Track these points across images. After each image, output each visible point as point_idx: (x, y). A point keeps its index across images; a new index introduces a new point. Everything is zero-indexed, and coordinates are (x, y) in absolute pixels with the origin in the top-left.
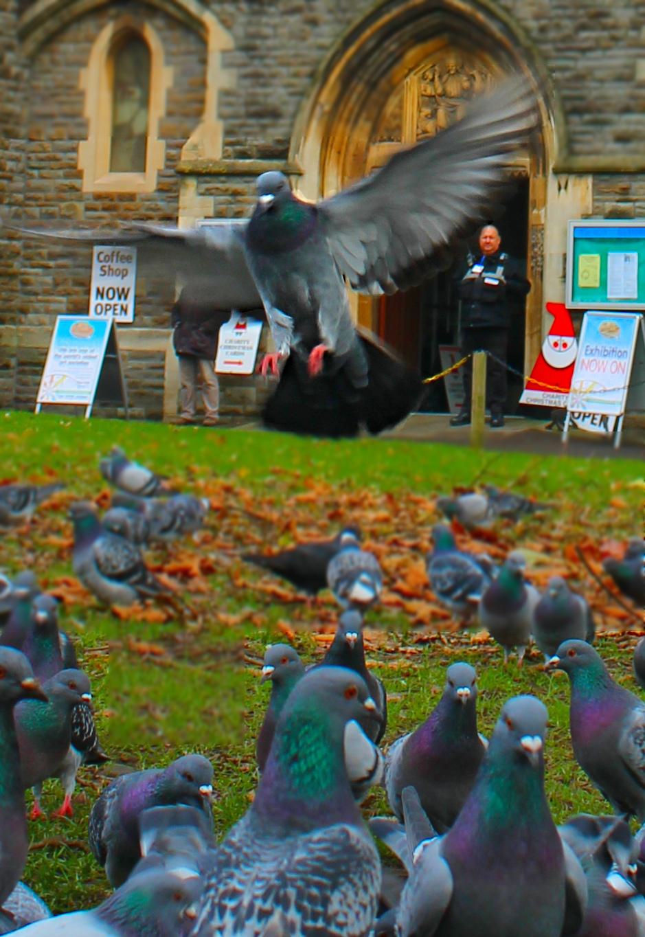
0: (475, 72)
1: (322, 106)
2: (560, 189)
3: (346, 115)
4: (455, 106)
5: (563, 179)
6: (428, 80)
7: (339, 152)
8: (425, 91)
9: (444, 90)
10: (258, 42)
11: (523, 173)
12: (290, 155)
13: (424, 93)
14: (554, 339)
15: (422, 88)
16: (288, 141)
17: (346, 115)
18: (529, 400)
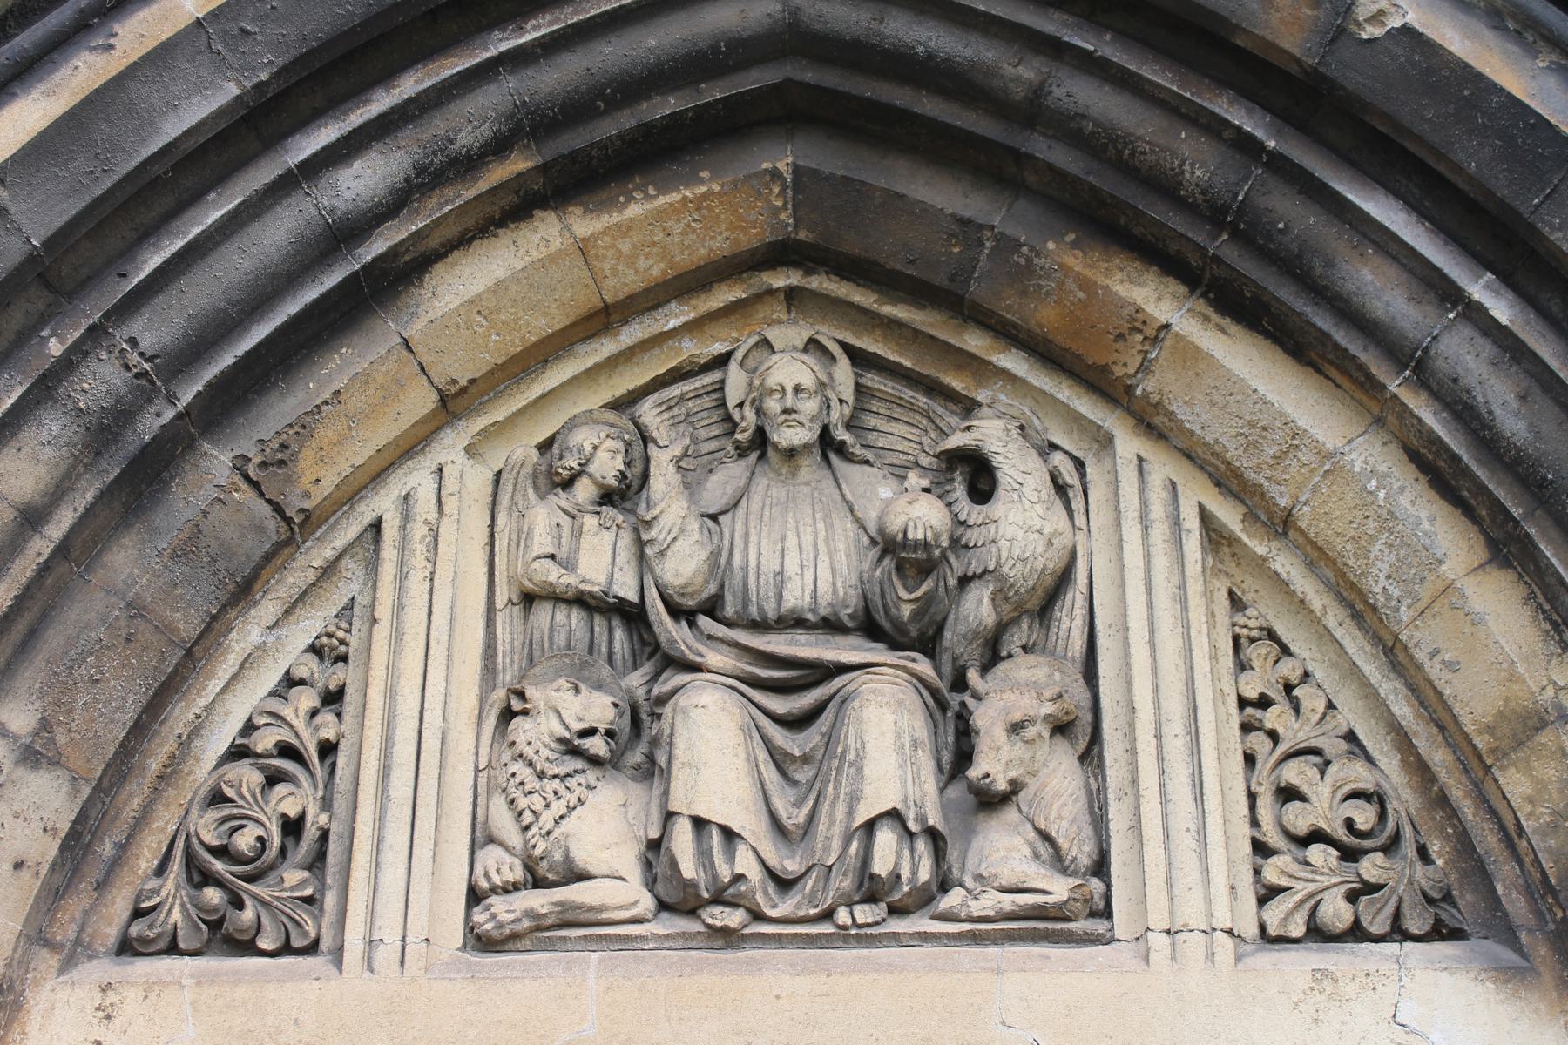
6: (584, 491)
8: (569, 565)
9: (718, 563)
13: (553, 575)
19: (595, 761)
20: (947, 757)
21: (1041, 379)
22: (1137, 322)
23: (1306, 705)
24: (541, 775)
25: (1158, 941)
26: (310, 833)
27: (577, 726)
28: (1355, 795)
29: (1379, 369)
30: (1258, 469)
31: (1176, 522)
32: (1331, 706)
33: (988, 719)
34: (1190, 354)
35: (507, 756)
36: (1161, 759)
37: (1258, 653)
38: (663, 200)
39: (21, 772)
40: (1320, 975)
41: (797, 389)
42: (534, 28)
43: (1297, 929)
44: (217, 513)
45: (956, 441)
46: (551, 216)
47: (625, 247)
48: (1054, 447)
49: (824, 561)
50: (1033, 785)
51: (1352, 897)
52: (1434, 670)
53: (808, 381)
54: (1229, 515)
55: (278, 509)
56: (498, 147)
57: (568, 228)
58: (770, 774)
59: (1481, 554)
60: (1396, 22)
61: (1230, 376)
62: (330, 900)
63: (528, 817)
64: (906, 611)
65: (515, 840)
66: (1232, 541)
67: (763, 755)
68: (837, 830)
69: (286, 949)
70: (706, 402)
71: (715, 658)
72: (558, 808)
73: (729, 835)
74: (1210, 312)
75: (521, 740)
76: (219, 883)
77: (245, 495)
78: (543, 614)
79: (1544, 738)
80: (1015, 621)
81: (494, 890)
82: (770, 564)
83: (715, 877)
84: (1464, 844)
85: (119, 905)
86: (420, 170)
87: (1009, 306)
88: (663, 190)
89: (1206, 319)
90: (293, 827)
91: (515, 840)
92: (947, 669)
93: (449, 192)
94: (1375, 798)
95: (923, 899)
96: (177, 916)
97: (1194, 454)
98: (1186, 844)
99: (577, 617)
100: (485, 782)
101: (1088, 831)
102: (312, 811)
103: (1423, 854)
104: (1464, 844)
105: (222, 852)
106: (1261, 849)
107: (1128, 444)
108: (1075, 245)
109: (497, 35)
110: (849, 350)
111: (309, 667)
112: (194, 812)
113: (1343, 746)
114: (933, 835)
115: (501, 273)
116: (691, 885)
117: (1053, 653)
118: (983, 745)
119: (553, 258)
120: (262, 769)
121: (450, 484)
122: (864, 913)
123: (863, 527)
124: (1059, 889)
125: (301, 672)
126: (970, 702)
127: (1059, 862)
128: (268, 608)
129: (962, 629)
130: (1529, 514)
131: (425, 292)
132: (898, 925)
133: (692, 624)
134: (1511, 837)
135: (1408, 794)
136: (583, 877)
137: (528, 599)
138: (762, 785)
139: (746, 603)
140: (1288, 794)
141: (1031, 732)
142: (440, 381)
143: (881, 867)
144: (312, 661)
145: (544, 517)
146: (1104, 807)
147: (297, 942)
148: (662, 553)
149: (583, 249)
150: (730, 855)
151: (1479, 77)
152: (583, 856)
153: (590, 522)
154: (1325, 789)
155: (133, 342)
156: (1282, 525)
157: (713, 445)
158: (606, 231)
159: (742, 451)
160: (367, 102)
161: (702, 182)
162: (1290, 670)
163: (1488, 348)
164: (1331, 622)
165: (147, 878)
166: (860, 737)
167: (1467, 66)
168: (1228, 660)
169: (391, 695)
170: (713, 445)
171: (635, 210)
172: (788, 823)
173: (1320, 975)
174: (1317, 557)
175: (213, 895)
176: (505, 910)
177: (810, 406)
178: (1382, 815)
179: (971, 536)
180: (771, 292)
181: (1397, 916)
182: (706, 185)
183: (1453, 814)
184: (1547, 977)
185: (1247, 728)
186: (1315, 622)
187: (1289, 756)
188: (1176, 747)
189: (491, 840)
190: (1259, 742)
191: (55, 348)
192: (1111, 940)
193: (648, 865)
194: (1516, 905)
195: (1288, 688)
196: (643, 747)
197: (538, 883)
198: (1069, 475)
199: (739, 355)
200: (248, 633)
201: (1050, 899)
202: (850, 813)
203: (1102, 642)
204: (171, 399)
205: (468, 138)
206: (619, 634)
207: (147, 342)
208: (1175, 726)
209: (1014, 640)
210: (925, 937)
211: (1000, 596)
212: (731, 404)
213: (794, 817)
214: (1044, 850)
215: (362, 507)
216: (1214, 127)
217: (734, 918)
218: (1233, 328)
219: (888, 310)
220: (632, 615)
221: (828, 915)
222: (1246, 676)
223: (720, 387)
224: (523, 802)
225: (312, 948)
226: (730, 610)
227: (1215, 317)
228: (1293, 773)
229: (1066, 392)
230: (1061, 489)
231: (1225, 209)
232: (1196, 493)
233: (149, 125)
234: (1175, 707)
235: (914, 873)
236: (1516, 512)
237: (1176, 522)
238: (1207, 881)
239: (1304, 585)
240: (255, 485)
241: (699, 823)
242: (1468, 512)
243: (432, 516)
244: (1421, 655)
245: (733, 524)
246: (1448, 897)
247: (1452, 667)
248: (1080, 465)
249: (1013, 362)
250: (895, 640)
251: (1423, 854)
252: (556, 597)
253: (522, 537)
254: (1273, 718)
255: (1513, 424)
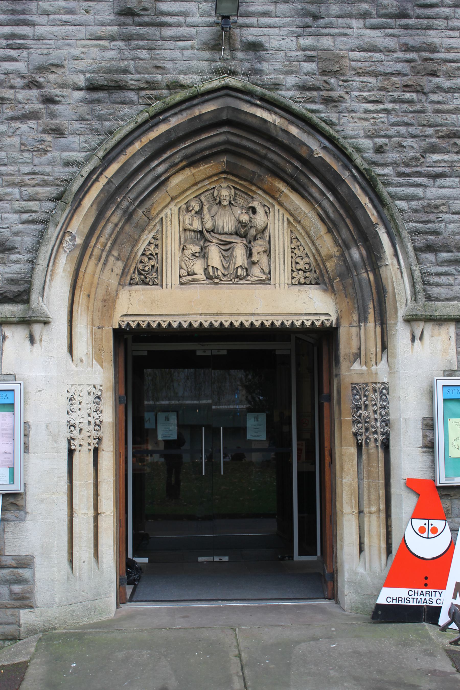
0: (256, 204)
1: (74, 238)
2: (413, 339)
3: (97, 252)
4: (230, 243)
5: (418, 327)
6: (193, 212)
7: (89, 296)
8: (191, 225)
9: (214, 224)
10: (300, 30)
11: (326, 322)
12: (35, 297)
13: (190, 227)
14: (418, 523)
15: (187, 222)
16: (29, 281)
17: (97, 252)
18: (389, 600)
19: (197, 257)
20: (248, 255)
21: (264, 195)
22: (279, 190)
23: (300, 249)
24: (189, 259)
25: (277, 285)
26: (156, 267)
27: (194, 252)
28: (306, 263)
29: (314, 203)
30: (296, 214)
31: (283, 220)
32: (304, 249)
33: (254, 251)
34: (286, 196)
35: (184, 256)
36: (279, 258)
37: (294, 241)
38: (206, 166)
39: (117, 262)
40: (299, 290)
41: (226, 196)
42: (188, 143)
43: (297, 283)
44: (140, 220)
45: (250, 205)
46: (188, 169)
47: (200, 174)
48: (265, 206)
49: (230, 224)
50: (260, 261)
51: (305, 278)
52: (318, 247)
53: (228, 194)
54: (291, 219)
55: (148, 218)
56: (181, 161)
57: (191, 171)
58: (223, 259)
59: (327, 231)
60: (319, 155)
61: (292, 200)
62: (159, 277)
63: (188, 266)
64: (242, 232)
65: (186, 269)
66: (291, 223)
67: (221, 256)
68: (232, 268)
69: (154, 284)
70: (211, 195)
71: (214, 241)
72: (192, 264)
73: (217, 269)
74: (290, 189)
75: (186, 254)
76: (143, 275)
77: (144, 217)
78: (188, 233)
79: (332, 259)
80: (259, 234)
81: (183, 276)
82: (222, 225)
83: (215, 275)
84: (321, 271)
85: (129, 278)
86: (170, 166)
87: (259, 184)
88: (206, 165)
89: (290, 190)
90: (153, 266)
91: (186, 269)
92: (248, 241)
93: (174, 168)
94: (309, 264)
95: (244, 278)
96: (137, 280)
97: (286, 209)
98: (282, 271)
99: (193, 233)
100: (181, 260)
101: (268, 267)
102: (155, 264)
103: (315, 272)
104: (321, 271)
105: (143, 270)
106: (292, 271)
107: (277, 207)
108: (270, 176)
109: (182, 144)
110: (234, 187)
111: (153, 241)
112: (138, 264)
113: (305, 256)
114: (246, 269)
115: (181, 179)
116: (212, 276)
117: (264, 239)
118: (254, 255)
119: (189, 176)
120: (148, 257)
121: (173, 212)
122: (236, 280)
123: (236, 218)
124: (264, 277)
125: (152, 242)
126: (252, 247)
127: (264, 273)
128: (146, 232)
129: (250, 235)
130: (333, 228)
131: (169, 182)
132: (241, 282)
133: (210, 233)
134: (327, 271)
135: (314, 263)
136: (196, 274)
137: (185, 230)
138: (222, 263)
139: (218, 230)
140: (297, 263)
141: (261, 253)
142: (171, 196)
143: (239, 274)
144: (153, 239)
145: (188, 217)
146: (271, 263)
147: (155, 284)
148: (206, 223)
149: (193, 175)
150: (217, 272)
151: (330, 166)
152: (196, 271)
153: (195, 218)
154: (302, 263)
155: (129, 197)
156: (299, 222)
157: (212, 202)
158: (197, 172)
159: (217, 204)
160: (162, 156)
161: (212, 163)
162: (298, 243)
163: (329, 203)
164: (305, 237)
165: (132, 274)
166: (236, 254)
167: (329, 164)
168: (290, 242)
169: (166, 247)
170: (212, 202)
171: (201, 168)
172: (225, 266)
173: (299, 290)
174: (303, 228)
175: (143, 277)
176: (185, 279)
177: (228, 198)
178: (310, 266)
179: (252, 220)
180: (222, 178)
181: (311, 281)
182: (212, 164)
183: (320, 267)
184: (330, 291)
185: (292, 252)
186: (303, 237)
187: (297, 257)
188: (281, 256)
189: (182, 268)
190: (293, 255)
191: (119, 200)
192: (270, 284)
193: (205, 272)
194: (327, 280)
195: (298, 246)
196: (203, 253)
197: (189, 275)
198: (268, 211)
199: (216, 188)
200: (144, 236)
201: (262, 279)
202: (234, 266)
203: (271, 238)
204: (134, 204)
205: (177, 161)
206: (199, 235)
207: (131, 197)
208: (281, 253)
209: (258, 237)
210: (245, 283)
211: (256, 230)
212: (215, 196)
213: (226, 266)
214: (262, 271)
215: (159, 215)
216: (292, 164)
217: (218, 281)
218: (294, 192)
219: (240, 182)
220: (201, 232)
221: (231, 280)
222: (292, 244)
223: (213, 192)
224: (187, 263)
225: (157, 284)
226: (215, 231)
227: (291, 190)
228: (298, 260)
229: (268, 198)
230: (266, 213)
231: (293, 176)
232: (287, 216)
233: (132, 166)
234: (281, 250)
235: (243, 274)
236: (331, 227)
237: (283, 220)
238: (285, 277)
239: (301, 231)
240: (145, 215)
241: (213, 267)
242: (326, 225)
243: (170, 217)
244: (317, 244)
245: (216, 217)
246: (318, 278)
247: (321, 247)
248: (269, 209)
249: (259, 192)
250: (241, 236)
251: (315, 272)
252: (190, 230)
253: (184, 220)
254: (296, 251)
255: (332, 215)
